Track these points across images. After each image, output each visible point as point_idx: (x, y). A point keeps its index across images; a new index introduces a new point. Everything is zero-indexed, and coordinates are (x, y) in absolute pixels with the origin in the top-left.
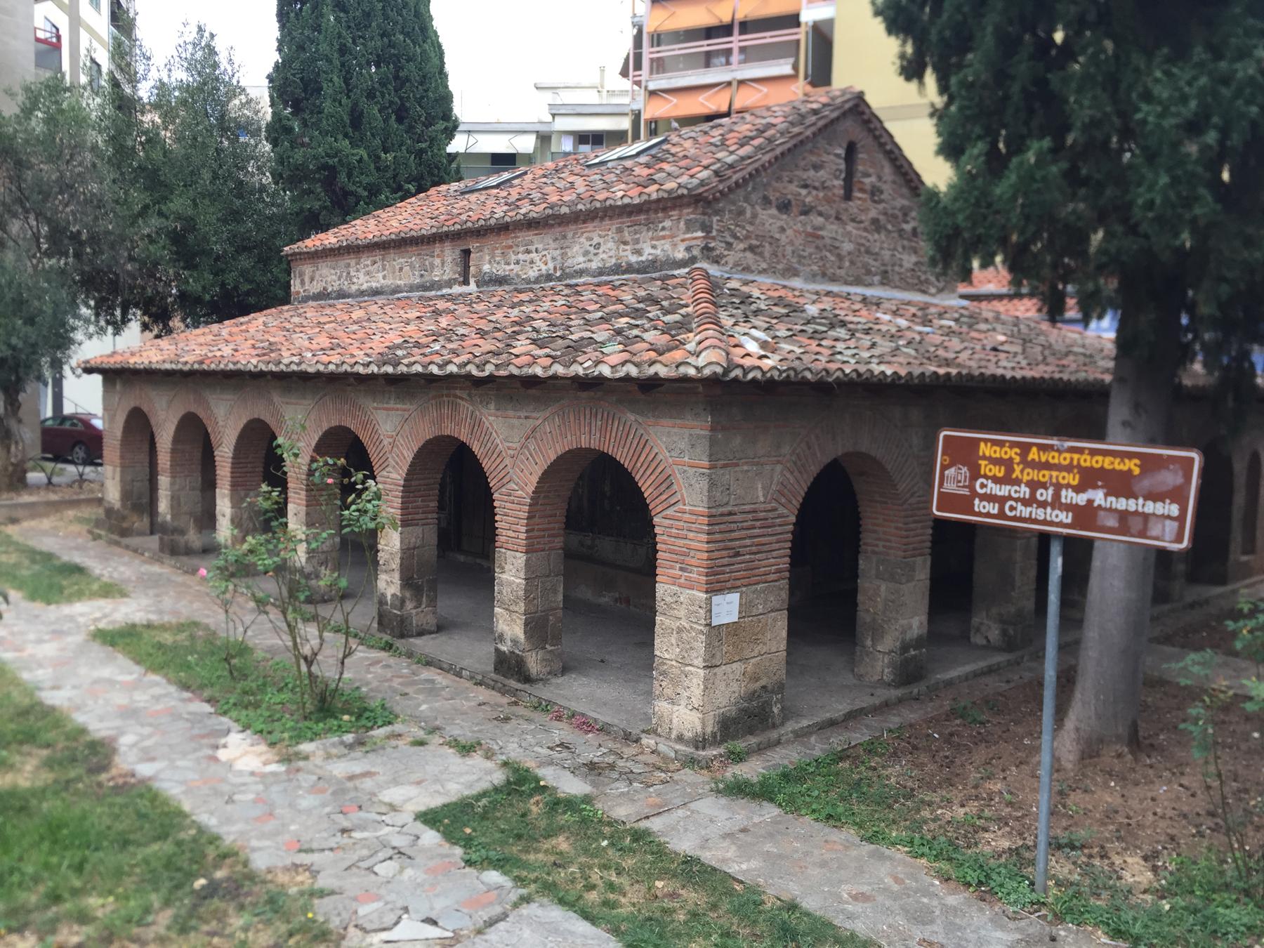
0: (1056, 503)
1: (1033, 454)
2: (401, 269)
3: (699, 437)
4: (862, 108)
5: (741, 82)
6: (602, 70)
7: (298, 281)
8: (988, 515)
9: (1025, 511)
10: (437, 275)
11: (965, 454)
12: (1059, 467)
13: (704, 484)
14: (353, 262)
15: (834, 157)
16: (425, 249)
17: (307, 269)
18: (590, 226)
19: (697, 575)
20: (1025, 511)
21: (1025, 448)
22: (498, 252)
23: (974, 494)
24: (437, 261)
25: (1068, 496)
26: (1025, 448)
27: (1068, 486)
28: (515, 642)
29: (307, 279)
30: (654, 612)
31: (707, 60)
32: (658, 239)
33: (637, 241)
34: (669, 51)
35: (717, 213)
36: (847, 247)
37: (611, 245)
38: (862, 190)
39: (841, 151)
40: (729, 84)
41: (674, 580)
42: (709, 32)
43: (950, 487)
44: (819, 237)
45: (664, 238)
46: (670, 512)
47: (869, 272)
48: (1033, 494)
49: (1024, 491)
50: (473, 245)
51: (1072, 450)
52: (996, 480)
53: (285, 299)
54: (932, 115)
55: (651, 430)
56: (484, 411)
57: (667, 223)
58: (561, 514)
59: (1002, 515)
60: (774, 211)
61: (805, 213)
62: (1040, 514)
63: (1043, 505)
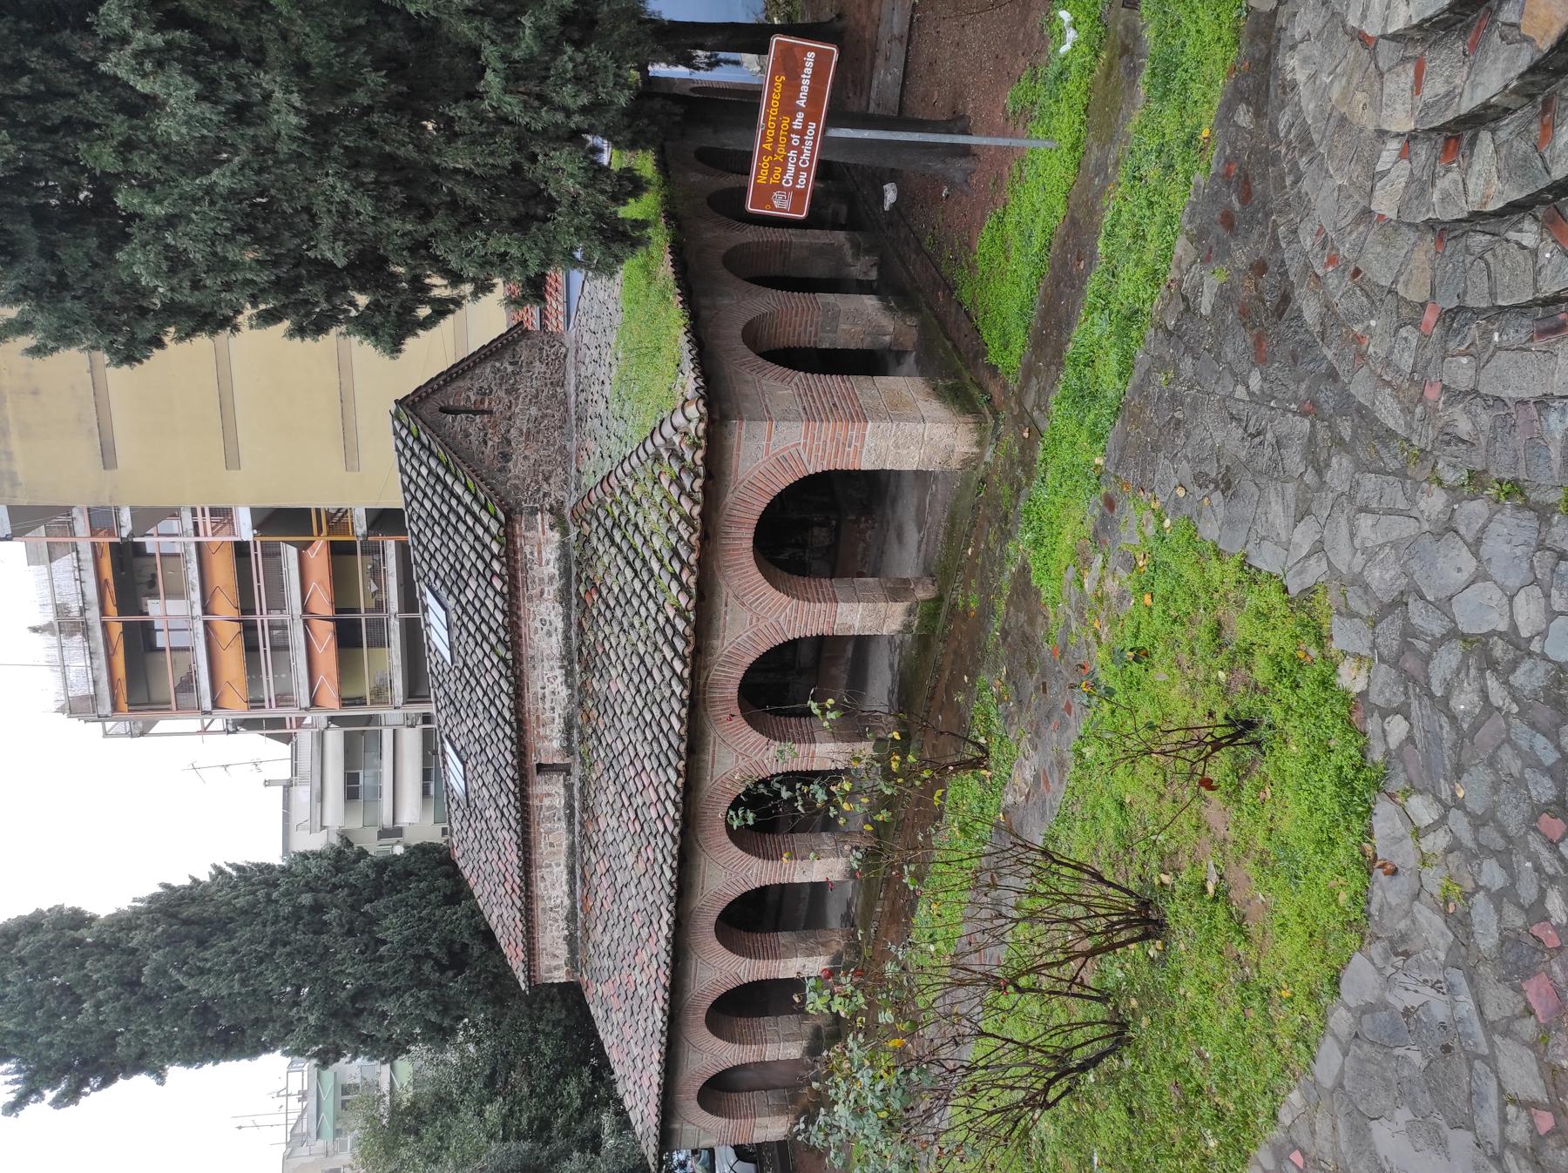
0: (802, 133)
1: (768, 147)
2: (552, 845)
3: (748, 432)
4: (409, 401)
5: (305, 609)
6: (267, 783)
7: (556, 974)
8: (807, 179)
9: (807, 154)
10: (559, 802)
11: (765, 193)
12: (778, 129)
13: (783, 426)
14: (541, 905)
15: (457, 423)
16: (535, 816)
17: (544, 962)
18: (524, 630)
19: (854, 431)
20: (807, 154)
21: (763, 152)
22: (541, 730)
23: (793, 188)
24: (547, 802)
25: (797, 125)
26: (763, 152)
27: (790, 124)
28: (910, 612)
29: (555, 963)
30: (883, 470)
31: (280, 648)
32: (540, 559)
33: (542, 580)
34: (269, 691)
35: (519, 504)
36: (534, 411)
37: (542, 609)
38: (482, 402)
39: (450, 418)
40: (306, 622)
41: (858, 452)
42: (251, 648)
43: (787, 205)
44: (529, 432)
45: (540, 553)
46: (805, 457)
47: (554, 396)
48: (794, 148)
49: (792, 154)
50: (534, 760)
51: (766, 120)
52: (784, 173)
53: (572, 996)
54: (399, 351)
55: (740, 478)
56: (719, 651)
57: (527, 549)
58: (801, 580)
59: (808, 170)
60: (511, 464)
61: (509, 442)
62: (809, 144)
63: (802, 142)
